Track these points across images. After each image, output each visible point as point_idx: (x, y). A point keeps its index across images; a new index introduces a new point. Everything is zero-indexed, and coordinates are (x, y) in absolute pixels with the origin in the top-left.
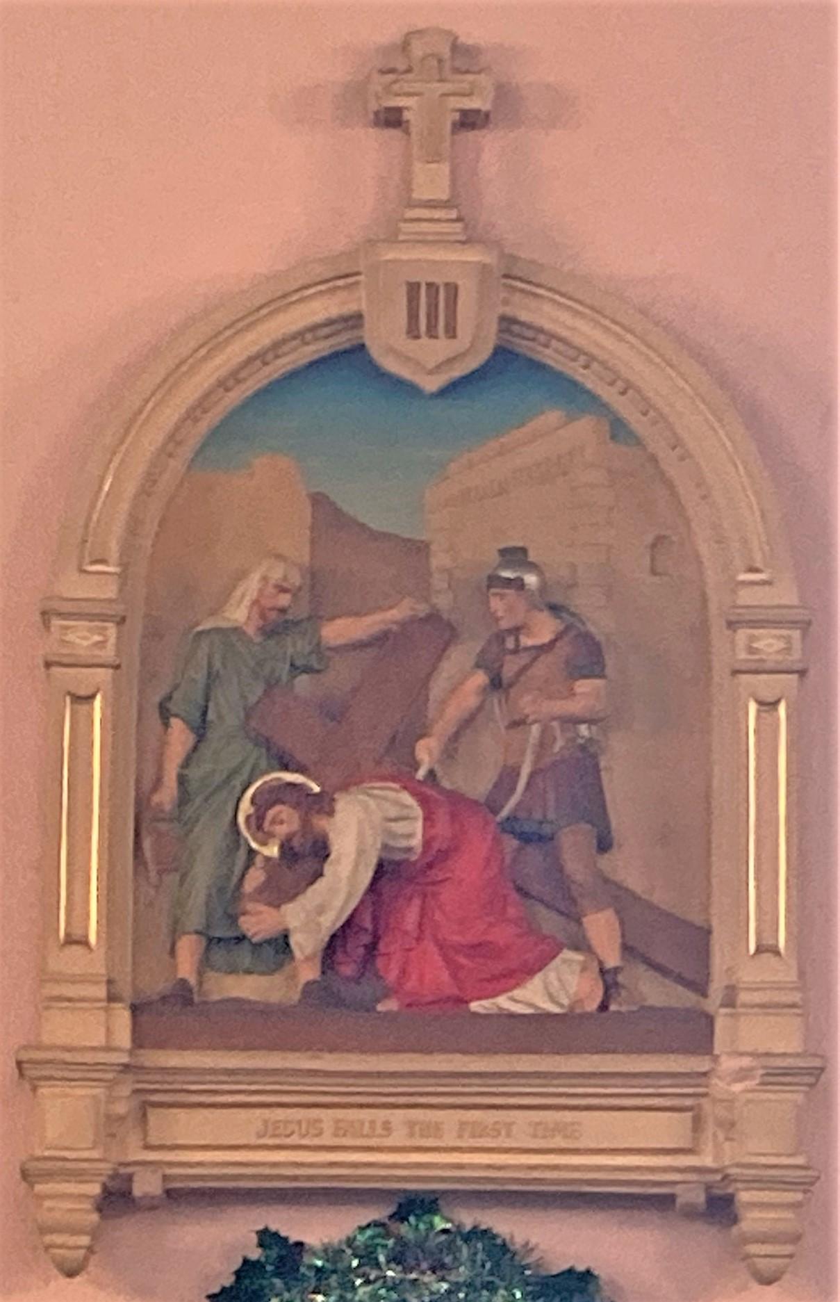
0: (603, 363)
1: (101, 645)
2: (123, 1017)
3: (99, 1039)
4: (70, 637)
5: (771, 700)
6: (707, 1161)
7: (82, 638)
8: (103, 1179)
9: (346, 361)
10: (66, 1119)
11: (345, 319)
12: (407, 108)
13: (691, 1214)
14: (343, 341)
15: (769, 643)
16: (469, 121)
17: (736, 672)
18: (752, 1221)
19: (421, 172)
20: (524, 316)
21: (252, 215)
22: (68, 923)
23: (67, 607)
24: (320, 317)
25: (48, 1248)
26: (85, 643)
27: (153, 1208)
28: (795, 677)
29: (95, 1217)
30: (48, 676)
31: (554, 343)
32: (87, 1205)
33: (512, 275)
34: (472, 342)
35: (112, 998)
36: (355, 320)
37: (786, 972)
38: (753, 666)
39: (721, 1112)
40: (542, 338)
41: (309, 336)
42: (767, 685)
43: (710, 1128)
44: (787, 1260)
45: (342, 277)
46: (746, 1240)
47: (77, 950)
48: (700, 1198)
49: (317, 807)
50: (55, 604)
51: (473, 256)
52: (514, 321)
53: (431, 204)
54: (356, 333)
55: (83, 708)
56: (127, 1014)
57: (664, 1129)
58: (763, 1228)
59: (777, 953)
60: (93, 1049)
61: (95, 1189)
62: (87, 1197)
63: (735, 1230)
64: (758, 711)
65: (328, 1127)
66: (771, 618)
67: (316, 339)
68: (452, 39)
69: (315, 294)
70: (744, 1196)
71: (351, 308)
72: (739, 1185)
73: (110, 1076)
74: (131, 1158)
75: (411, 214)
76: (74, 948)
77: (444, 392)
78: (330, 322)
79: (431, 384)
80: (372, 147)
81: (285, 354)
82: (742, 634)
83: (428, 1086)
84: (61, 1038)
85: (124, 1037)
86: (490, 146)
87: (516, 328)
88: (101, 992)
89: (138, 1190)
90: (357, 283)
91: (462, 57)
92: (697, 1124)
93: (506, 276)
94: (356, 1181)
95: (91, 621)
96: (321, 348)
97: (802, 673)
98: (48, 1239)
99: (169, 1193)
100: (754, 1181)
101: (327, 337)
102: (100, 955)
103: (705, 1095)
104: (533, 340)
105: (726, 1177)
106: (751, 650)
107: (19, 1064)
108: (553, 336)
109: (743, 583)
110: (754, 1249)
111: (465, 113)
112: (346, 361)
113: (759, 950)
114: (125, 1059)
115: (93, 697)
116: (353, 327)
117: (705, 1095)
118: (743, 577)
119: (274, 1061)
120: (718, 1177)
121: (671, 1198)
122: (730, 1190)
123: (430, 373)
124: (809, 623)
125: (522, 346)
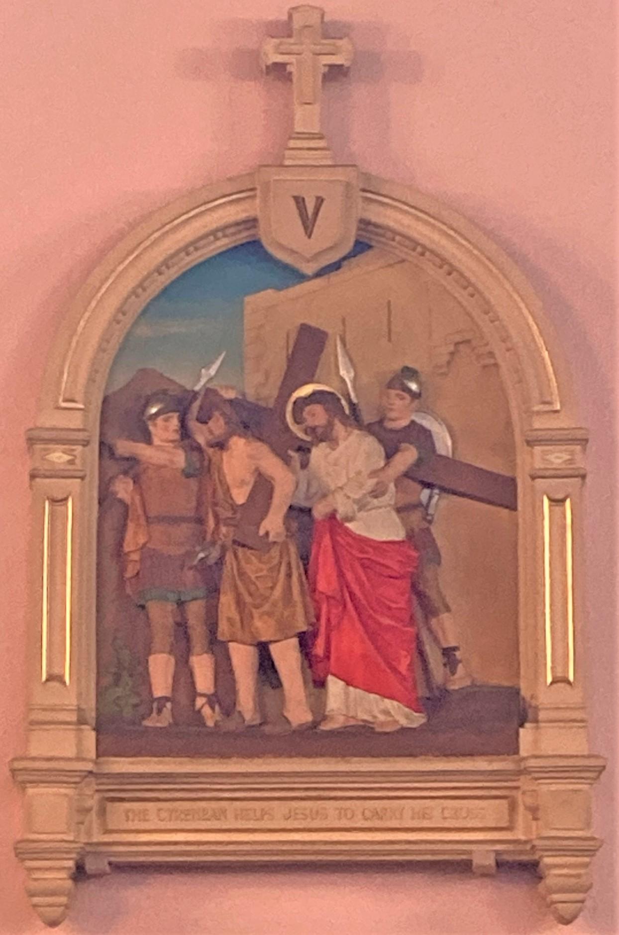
0: (432, 252)
1: (71, 462)
2: (90, 737)
3: (71, 752)
4: (67, 458)
5: (60, 497)
6: (519, 835)
8: (74, 856)
9: (249, 250)
10: (52, 811)
11: (245, 222)
13: (485, 874)
14: (243, 237)
15: (557, 458)
16: (335, 73)
17: (533, 478)
18: (552, 878)
19: (299, 113)
20: (374, 219)
21: (167, 150)
22: (49, 665)
23: (46, 435)
24: (232, 219)
25: (35, 906)
26: (560, 461)
27: (484, 875)
28: (79, 480)
29: (69, 883)
30: (31, 487)
31: (398, 238)
33: (369, 189)
34: (333, 231)
35: (81, 721)
36: (251, 223)
38: (570, 472)
39: (529, 801)
41: (220, 234)
42: (57, 487)
43: (521, 809)
44: (579, 905)
45: (247, 187)
46: (551, 891)
47: (55, 684)
48: (491, 861)
50: (36, 433)
51: (341, 175)
52: (368, 223)
53: (312, 137)
54: (252, 232)
55: (59, 508)
57: (491, 811)
58: (561, 881)
61: (71, 864)
62: (64, 868)
63: (541, 887)
64: (550, 506)
65: (437, 813)
66: (579, 437)
67: (225, 236)
69: (224, 203)
70: (547, 860)
71: (251, 214)
73: (77, 779)
74: (95, 840)
75: (292, 144)
76: (559, 685)
77: (319, 274)
78: (237, 224)
80: (253, 96)
81: (203, 247)
82: (538, 449)
83: (295, 783)
86: (359, 93)
87: (371, 228)
89: (477, 861)
91: (331, 31)
92: (513, 807)
93: (364, 190)
95: (64, 444)
96: (223, 243)
97: (82, 478)
98: (36, 900)
99: (499, 864)
100: (560, 850)
101: (234, 234)
104: (383, 236)
105: (533, 847)
107: (13, 771)
108: (395, 232)
109: (538, 413)
110: (556, 897)
111: (332, 67)
112: (249, 250)
113: (50, 678)
114: (90, 766)
115: (66, 499)
118: (536, 408)
119: (342, 766)
120: (528, 847)
122: (536, 857)
123: (308, 261)
124: (587, 440)
125: (361, 240)
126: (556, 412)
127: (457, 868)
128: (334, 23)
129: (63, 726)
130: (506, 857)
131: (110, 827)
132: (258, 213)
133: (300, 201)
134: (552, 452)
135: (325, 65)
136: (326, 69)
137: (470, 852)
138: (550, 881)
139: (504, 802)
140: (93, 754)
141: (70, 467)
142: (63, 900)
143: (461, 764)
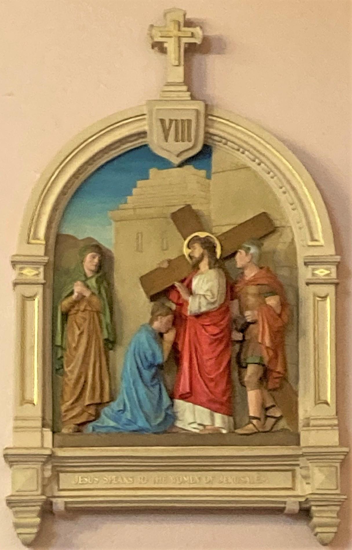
1: (37, 275)
4: (316, 272)
5: (323, 295)
6: (298, 492)
7: (29, 273)
8: (40, 504)
12: (166, 42)
17: (308, 284)
21: (131, 89)
31: (229, 143)
32: (35, 515)
35: (44, 426)
36: (143, 134)
37: (331, 411)
40: (224, 141)
48: (297, 508)
49: (276, 344)
56: (50, 433)
57: (281, 479)
59: (326, 403)
60: (35, 448)
61: (38, 508)
62: (334, 511)
68: (182, 14)
70: (313, 508)
72: (312, 503)
73: (43, 460)
79: (177, 161)
82: (310, 267)
83: (96, 462)
84: (312, 443)
85: (48, 442)
88: (39, 424)
90: (144, 119)
92: (294, 477)
94: (212, 503)
102: (333, 406)
103: (298, 465)
106: (313, 274)
111: (190, 44)
116: (143, 138)
117: (298, 465)
121: (284, 508)
126: (322, 246)
127: (275, 511)
128: (189, 19)
129: (31, 429)
130: (70, 506)
131: (61, 487)
132: (146, 128)
133: (162, 121)
134: (317, 269)
135: (186, 43)
136: (187, 46)
137: (285, 503)
138: (315, 520)
139: (290, 473)
140: (50, 446)
141: (327, 277)
142: (334, 530)
143: (146, 451)
